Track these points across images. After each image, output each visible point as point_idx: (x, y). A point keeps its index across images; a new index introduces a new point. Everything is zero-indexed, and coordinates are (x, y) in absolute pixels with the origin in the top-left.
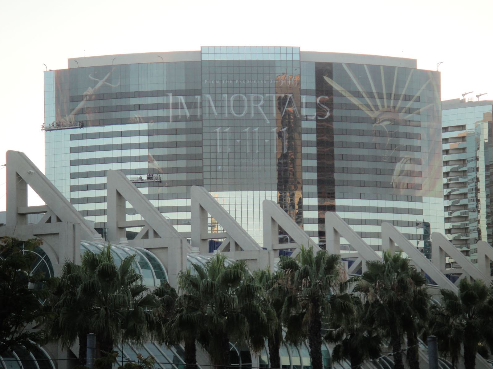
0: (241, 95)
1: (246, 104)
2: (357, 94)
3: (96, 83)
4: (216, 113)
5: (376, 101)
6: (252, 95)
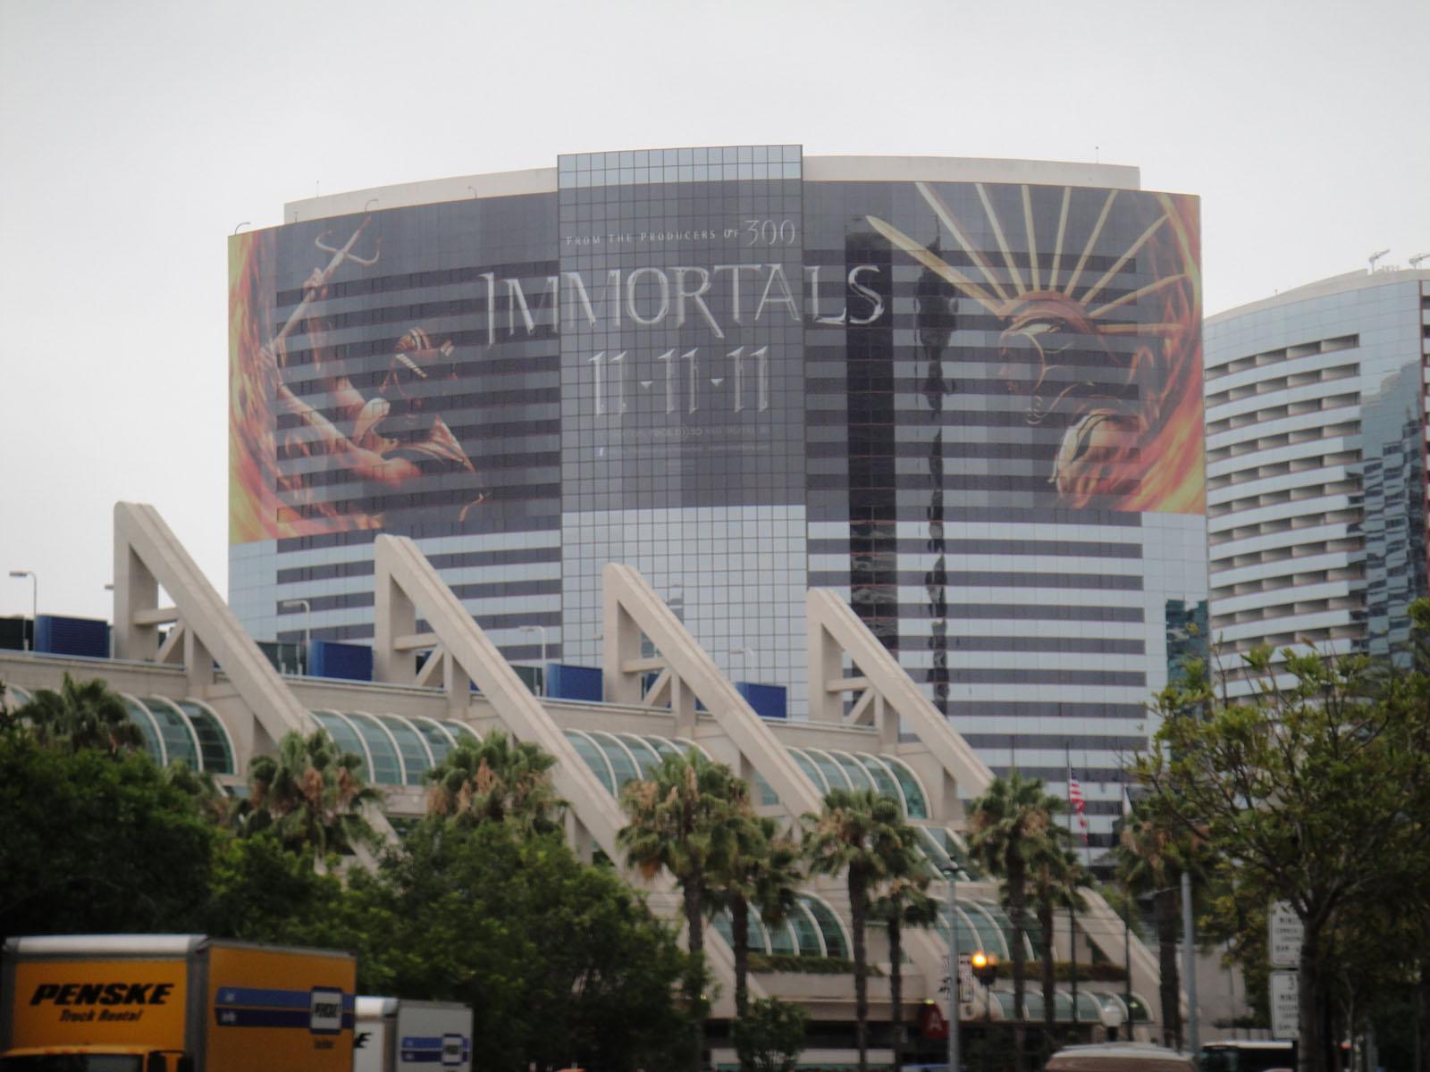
0: (654, 270)
1: (666, 294)
2: (959, 259)
3: (330, 256)
4: (592, 318)
5: (1008, 275)
6: (680, 269)
